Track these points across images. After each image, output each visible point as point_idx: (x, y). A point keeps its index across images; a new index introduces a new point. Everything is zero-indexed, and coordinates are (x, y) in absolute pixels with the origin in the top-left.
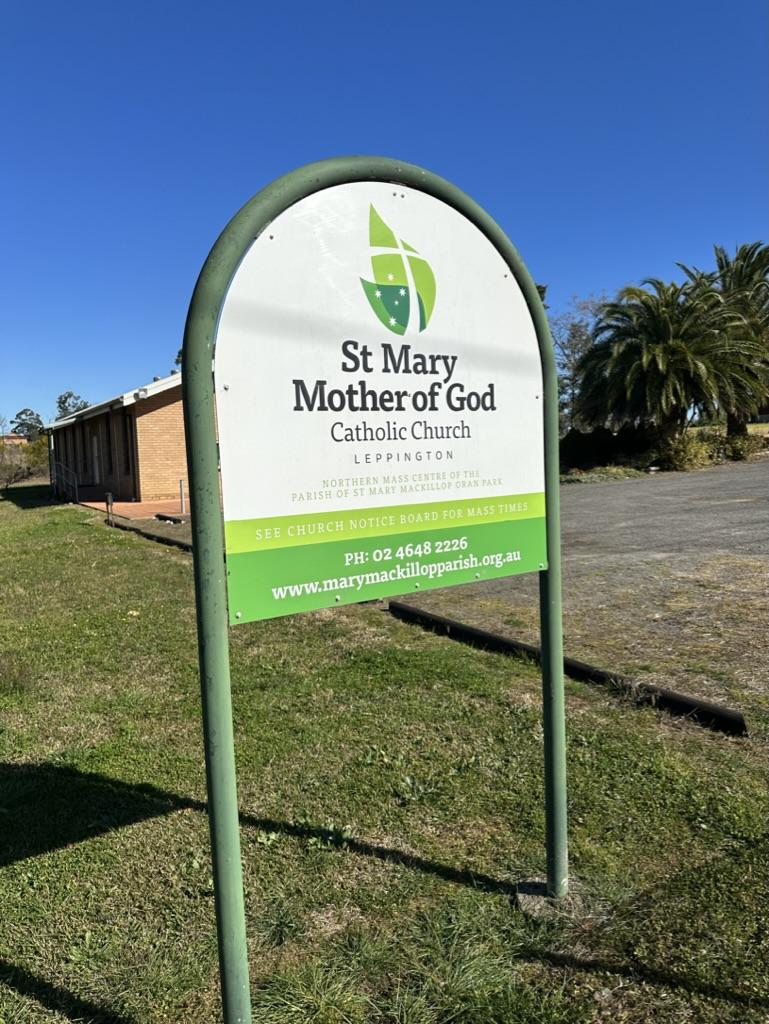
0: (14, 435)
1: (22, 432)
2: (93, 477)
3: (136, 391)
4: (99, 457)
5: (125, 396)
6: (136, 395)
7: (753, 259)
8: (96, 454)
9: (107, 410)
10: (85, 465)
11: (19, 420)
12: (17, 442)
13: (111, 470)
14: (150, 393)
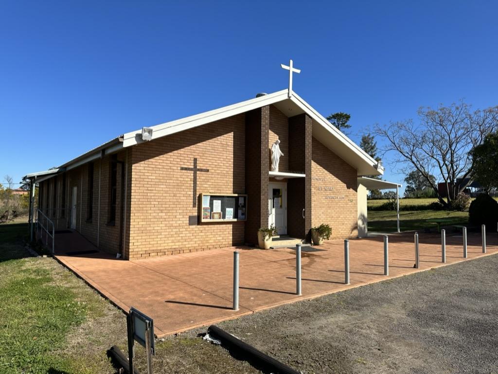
0: (21, 189)
1: (26, 188)
2: (70, 223)
3: (140, 132)
4: (78, 205)
5: (126, 136)
6: (139, 137)
7: (33, 195)
8: (75, 202)
9: (99, 155)
10: (63, 212)
11: (24, 182)
12: (21, 193)
13: (90, 218)
14: (156, 135)
